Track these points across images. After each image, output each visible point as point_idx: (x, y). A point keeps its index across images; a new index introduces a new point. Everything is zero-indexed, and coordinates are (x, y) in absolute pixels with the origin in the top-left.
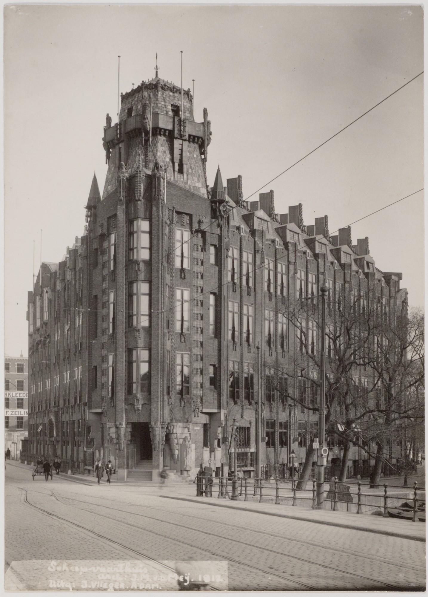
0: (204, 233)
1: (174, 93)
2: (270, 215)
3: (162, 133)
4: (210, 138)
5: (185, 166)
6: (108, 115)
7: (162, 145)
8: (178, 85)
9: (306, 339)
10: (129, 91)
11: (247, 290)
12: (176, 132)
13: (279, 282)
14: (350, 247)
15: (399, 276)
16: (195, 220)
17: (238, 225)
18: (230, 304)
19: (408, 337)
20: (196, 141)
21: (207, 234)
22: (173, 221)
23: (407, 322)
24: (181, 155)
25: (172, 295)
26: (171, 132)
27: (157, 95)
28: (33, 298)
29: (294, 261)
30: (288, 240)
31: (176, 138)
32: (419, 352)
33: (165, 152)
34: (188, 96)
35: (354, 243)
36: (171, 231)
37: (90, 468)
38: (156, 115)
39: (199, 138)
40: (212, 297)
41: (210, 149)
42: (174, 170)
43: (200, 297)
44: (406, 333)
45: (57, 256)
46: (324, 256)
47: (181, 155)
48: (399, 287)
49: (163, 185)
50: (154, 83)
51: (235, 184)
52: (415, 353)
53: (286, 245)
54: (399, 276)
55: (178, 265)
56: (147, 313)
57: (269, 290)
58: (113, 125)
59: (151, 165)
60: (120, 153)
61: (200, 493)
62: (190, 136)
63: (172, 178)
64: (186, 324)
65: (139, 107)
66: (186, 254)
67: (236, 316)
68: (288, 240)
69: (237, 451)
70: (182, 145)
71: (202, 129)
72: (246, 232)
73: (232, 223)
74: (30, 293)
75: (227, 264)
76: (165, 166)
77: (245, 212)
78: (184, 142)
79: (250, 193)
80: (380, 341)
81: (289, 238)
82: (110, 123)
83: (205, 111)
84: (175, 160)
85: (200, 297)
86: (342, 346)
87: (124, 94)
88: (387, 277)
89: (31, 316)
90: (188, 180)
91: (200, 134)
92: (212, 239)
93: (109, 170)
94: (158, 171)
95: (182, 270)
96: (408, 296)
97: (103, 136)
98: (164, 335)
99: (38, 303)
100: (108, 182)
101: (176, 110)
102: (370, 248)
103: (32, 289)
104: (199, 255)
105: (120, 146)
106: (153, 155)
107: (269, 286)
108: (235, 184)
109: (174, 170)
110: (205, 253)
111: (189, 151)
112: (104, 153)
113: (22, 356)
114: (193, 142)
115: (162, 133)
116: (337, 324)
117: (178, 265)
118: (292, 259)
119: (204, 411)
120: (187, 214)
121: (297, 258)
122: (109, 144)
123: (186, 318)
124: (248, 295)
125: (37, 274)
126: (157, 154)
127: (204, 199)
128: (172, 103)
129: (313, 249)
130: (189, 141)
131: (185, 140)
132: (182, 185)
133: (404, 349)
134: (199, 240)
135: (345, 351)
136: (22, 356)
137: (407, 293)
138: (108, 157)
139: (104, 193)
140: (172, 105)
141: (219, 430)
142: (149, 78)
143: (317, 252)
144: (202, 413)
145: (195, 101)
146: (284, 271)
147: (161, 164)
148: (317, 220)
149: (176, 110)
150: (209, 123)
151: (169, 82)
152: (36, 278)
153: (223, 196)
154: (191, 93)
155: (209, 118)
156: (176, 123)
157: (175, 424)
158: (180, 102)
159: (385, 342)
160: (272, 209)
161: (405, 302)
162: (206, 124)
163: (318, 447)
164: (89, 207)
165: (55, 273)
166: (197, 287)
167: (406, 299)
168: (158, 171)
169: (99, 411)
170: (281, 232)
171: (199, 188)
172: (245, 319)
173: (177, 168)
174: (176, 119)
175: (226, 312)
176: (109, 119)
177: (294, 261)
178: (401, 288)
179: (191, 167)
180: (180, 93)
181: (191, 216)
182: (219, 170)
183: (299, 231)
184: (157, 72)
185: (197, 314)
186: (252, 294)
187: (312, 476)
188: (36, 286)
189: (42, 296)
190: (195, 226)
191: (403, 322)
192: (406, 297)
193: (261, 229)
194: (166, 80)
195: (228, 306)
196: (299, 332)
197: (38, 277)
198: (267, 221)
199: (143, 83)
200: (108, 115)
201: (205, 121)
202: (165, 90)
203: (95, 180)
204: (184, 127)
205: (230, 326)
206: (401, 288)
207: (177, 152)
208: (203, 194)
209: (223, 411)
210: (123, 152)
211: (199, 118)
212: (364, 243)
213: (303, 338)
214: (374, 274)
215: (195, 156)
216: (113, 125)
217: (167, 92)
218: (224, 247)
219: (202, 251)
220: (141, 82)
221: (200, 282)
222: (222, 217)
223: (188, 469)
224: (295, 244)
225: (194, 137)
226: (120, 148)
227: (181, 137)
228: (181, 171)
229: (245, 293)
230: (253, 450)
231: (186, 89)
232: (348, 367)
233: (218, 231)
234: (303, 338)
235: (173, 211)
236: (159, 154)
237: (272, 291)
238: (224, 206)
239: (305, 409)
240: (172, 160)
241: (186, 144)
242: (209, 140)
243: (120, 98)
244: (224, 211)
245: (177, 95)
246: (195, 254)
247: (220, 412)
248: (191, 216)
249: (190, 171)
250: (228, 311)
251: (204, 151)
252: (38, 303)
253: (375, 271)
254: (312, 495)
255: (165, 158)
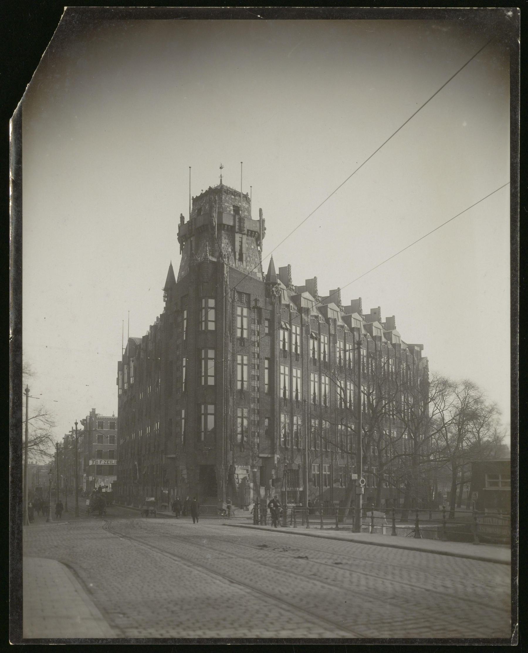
0: (259, 310)
1: (235, 196)
2: (314, 297)
3: (226, 228)
4: (264, 233)
5: (244, 255)
6: (181, 214)
7: (225, 239)
8: (238, 190)
9: (345, 395)
10: (199, 195)
11: (295, 358)
12: (237, 227)
13: (322, 351)
14: (380, 323)
15: (421, 347)
16: (252, 298)
17: (288, 303)
18: (282, 367)
19: (430, 394)
20: (253, 235)
21: (263, 311)
22: (234, 299)
23: (428, 384)
24: (241, 246)
25: (234, 360)
26: (233, 227)
27: (222, 198)
28: (121, 366)
29: (334, 333)
30: (329, 317)
31: (237, 233)
32: (439, 408)
33: (228, 244)
34: (247, 200)
35: (384, 320)
36: (233, 308)
37: (166, 504)
38: (220, 214)
39: (255, 232)
40: (266, 362)
41: (265, 242)
42: (235, 259)
43: (256, 361)
44: (427, 393)
45: (141, 331)
46: (359, 330)
47: (241, 246)
48: (421, 356)
49: (226, 269)
50: (219, 188)
51: (286, 272)
52: (436, 408)
53: (327, 320)
54: (421, 347)
55: (239, 335)
56: (213, 375)
57: (314, 356)
58: (185, 222)
59: (217, 254)
60: (191, 245)
61: (256, 522)
62: (248, 231)
63: (234, 265)
64: (245, 384)
65: (207, 207)
66: (245, 326)
67: (287, 378)
68: (329, 317)
69: (288, 489)
70: (242, 238)
71: (258, 225)
72: (294, 309)
73: (283, 302)
74: (119, 362)
75: (279, 335)
76: (228, 254)
77: (293, 294)
78: (243, 236)
79: (298, 280)
80: (406, 399)
81: (330, 315)
82: (184, 221)
83: (261, 210)
84: (236, 251)
85: (256, 361)
86: (374, 401)
87: (195, 197)
88: (411, 347)
89: (120, 381)
90: (247, 266)
91: (257, 229)
92: (266, 314)
93: (183, 259)
94: (222, 258)
95: (242, 338)
96: (429, 363)
97: (178, 232)
98: (227, 392)
99: (126, 371)
100: (182, 268)
101: (237, 210)
102: (397, 324)
103: (121, 359)
104: (255, 327)
105: (192, 239)
106: (218, 246)
107: (314, 353)
108: (286, 272)
109: (235, 259)
110: (261, 326)
111: (247, 243)
112: (178, 245)
113: (113, 415)
114: (251, 236)
115: (226, 228)
116: (370, 383)
117: (239, 335)
118: (332, 332)
119: (261, 455)
120: (246, 294)
121: (337, 332)
122: (183, 238)
123: (245, 378)
124: (296, 360)
125: (125, 347)
126: (221, 245)
127: (260, 282)
128: (234, 204)
129: (349, 324)
130: (247, 235)
131: (244, 234)
132: (241, 270)
133: (426, 404)
134: (254, 315)
135: (377, 406)
136: (113, 415)
137: (427, 361)
138: (181, 249)
139: (178, 278)
140: (234, 206)
141: (273, 472)
142: (215, 183)
143: (353, 326)
144: (258, 457)
145: (253, 203)
146: (326, 342)
147: (224, 253)
148: (352, 301)
149: (237, 210)
150: (264, 221)
151: (231, 187)
152: (124, 350)
153: (276, 280)
154: (249, 196)
155: (263, 217)
156: (237, 220)
157: (236, 466)
158: (240, 204)
159: (411, 400)
160: (316, 291)
161: (426, 368)
162: (262, 221)
163: (356, 478)
164: (166, 289)
165: (140, 345)
166: (254, 353)
167: (427, 366)
168: (222, 258)
169: (174, 456)
170: (323, 310)
171: (256, 273)
172: (294, 380)
173: (237, 257)
174: (237, 217)
175: (278, 374)
176: (182, 218)
177: (334, 333)
178: (422, 357)
179: (249, 256)
180: (240, 196)
181: (249, 295)
182: (272, 258)
183: (338, 310)
184: (221, 180)
185: (254, 376)
186: (300, 360)
187: (351, 512)
188: (124, 357)
189: (129, 365)
190: (253, 304)
191: (426, 384)
192: (427, 363)
193: (306, 306)
194: (228, 186)
195: (280, 369)
196: (339, 389)
197: (126, 349)
198: (312, 301)
199: (210, 188)
200: (181, 214)
201: (260, 218)
202: (227, 194)
203: (171, 268)
204: (244, 223)
205: (282, 386)
206: (422, 357)
207: (237, 244)
208: (259, 278)
209: (277, 456)
210: (193, 244)
211: (255, 216)
212: (391, 321)
213: (342, 394)
214: (400, 345)
215: (253, 247)
216: (185, 222)
217: (229, 196)
218: (276, 320)
219: (258, 324)
220: (208, 187)
221: (257, 350)
222: (275, 296)
223: (246, 504)
224: (335, 319)
225: (252, 231)
226: (191, 241)
227: (241, 231)
228: (241, 259)
229: (294, 359)
230: (301, 489)
231: (245, 193)
232: (380, 419)
233: (270, 308)
234: (342, 394)
235: (234, 291)
236: (223, 245)
237: (316, 357)
238: (276, 288)
239: (345, 454)
240: (234, 250)
241: (245, 237)
242: (264, 234)
243: (192, 201)
244: (276, 292)
245: (237, 198)
246: (253, 327)
247: (274, 457)
248: (249, 295)
249: (248, 259)
250: (280, 373)
251: (260, 243)
252: (126, 371)
253: (401, 343)
254: (352, 521)
255: (228, 249)
